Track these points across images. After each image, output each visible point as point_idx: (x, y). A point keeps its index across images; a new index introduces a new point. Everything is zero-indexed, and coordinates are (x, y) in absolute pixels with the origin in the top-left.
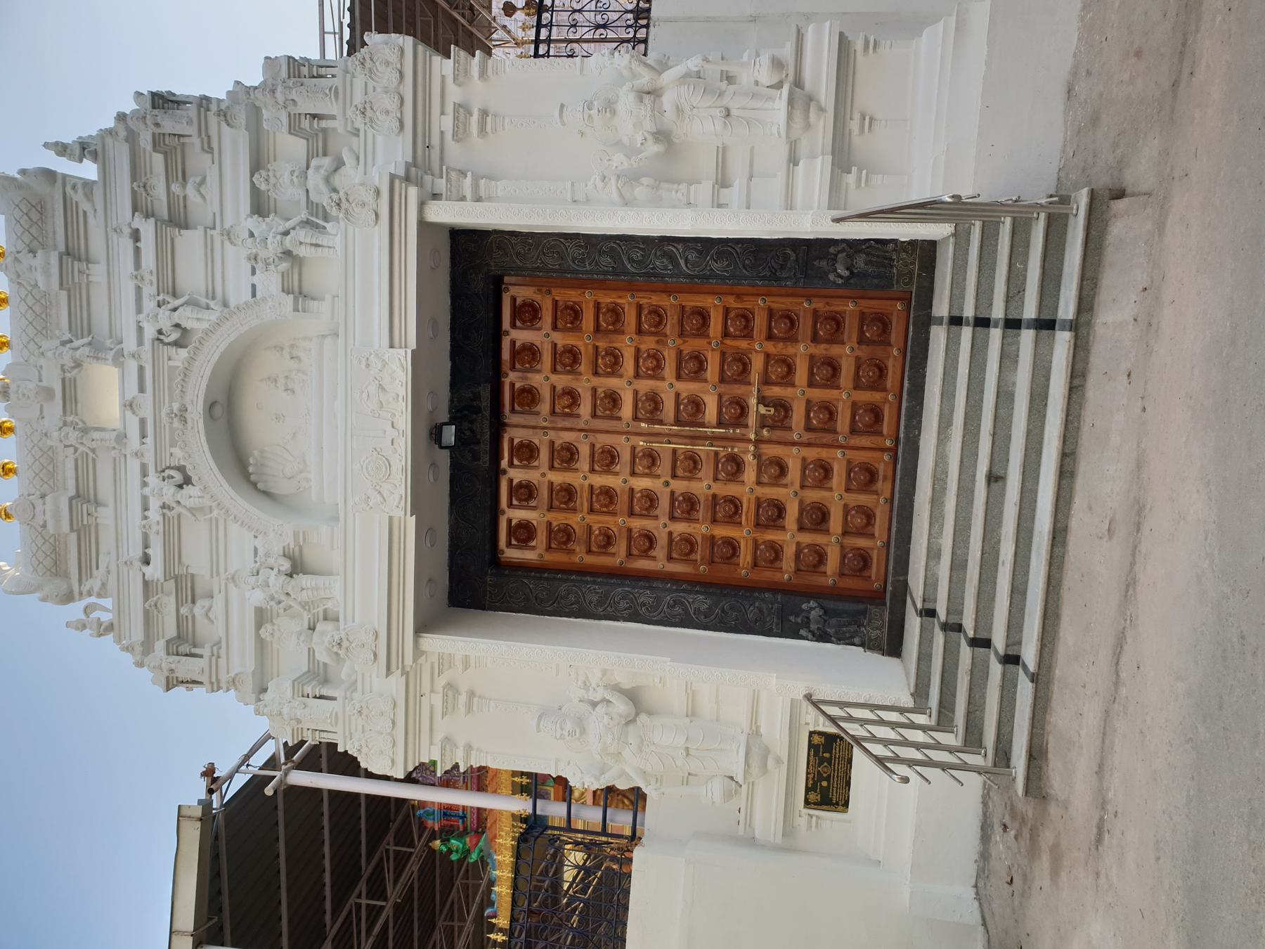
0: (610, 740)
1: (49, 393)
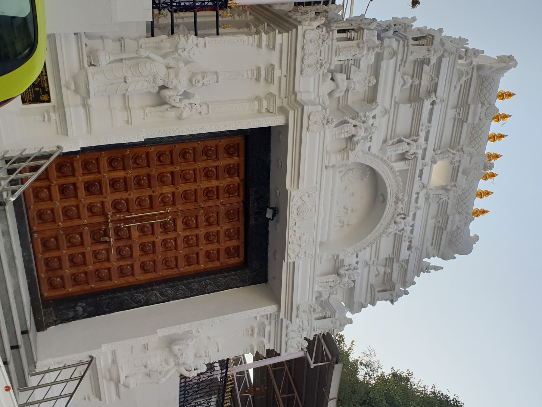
0: (174, 81)
1: (464, 173)
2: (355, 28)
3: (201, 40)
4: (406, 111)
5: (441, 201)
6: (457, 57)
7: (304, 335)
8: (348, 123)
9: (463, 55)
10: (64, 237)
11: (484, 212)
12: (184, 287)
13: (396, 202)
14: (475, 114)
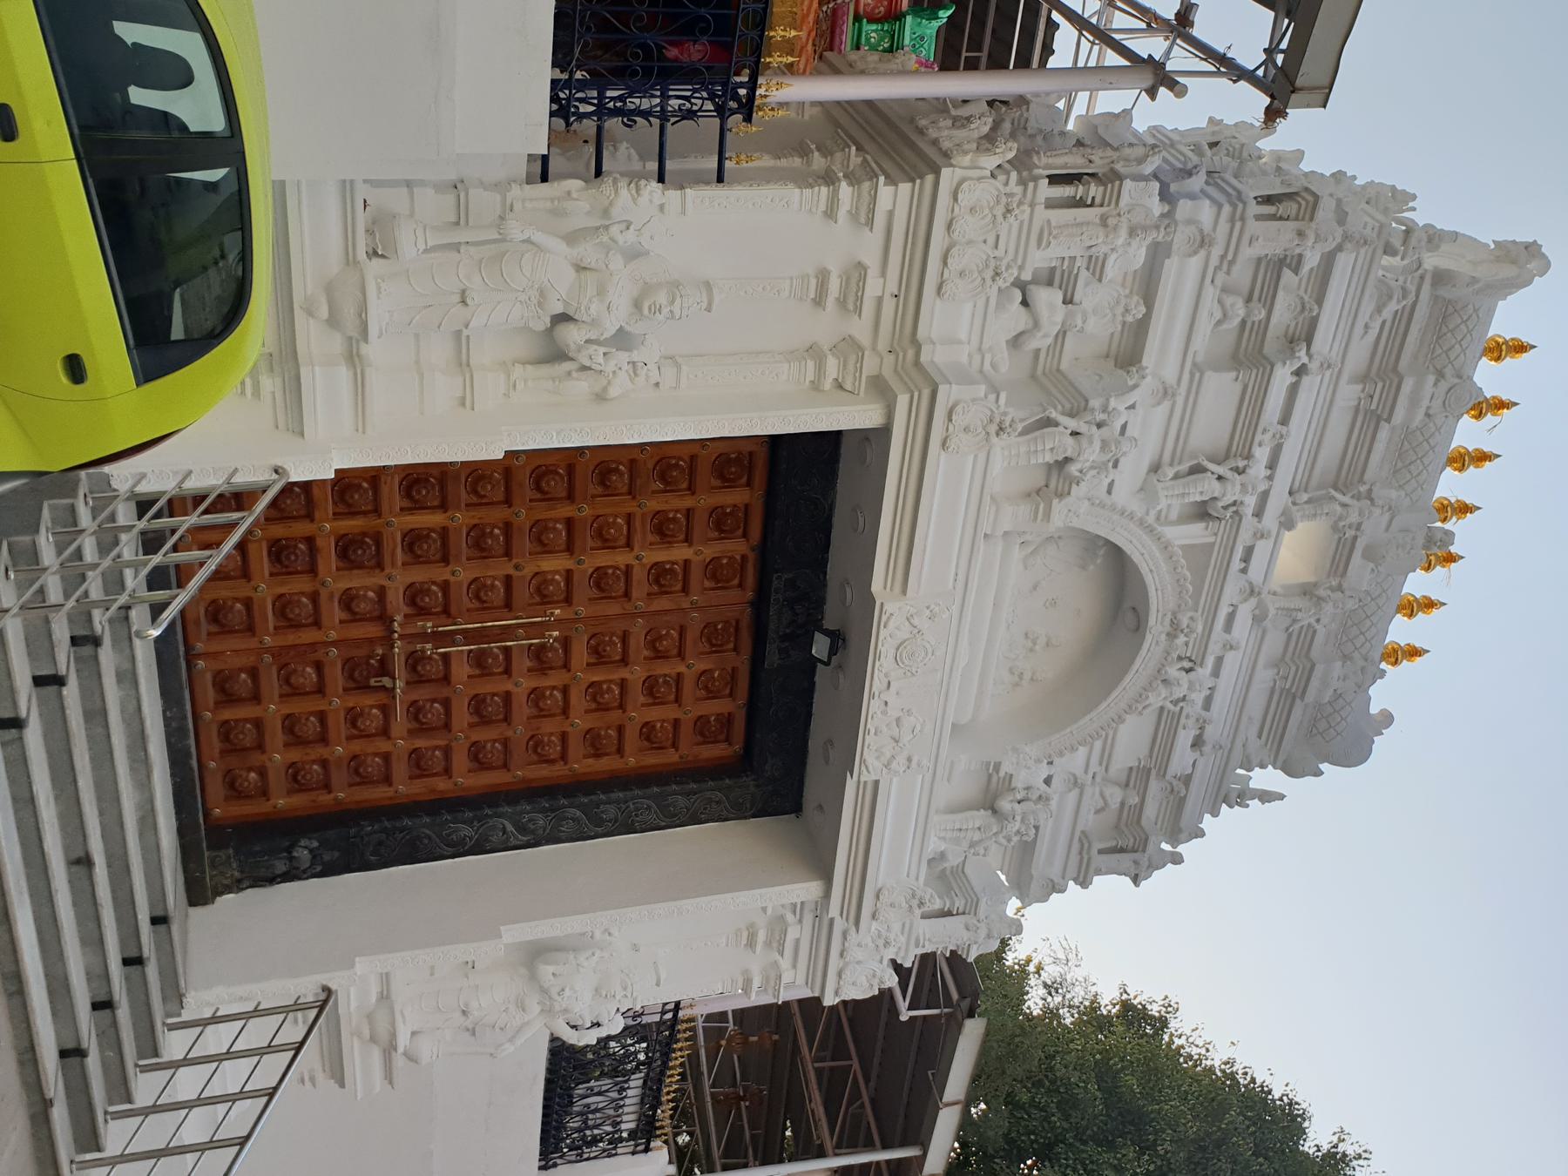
0: (593, 307)
1: (1369, 554)
2: (1100, 171)
3: (673, 195)
4: (1220, 392)
5: (1297, 626)
6: (1380, 251)
7: (890, 954)
8: (1057, 424)
9: (1397, 242)
10: (274, 670)
11: (1414, 652)
12: (578, 813)
13: (1171, 636)
14: (1414, 401)
